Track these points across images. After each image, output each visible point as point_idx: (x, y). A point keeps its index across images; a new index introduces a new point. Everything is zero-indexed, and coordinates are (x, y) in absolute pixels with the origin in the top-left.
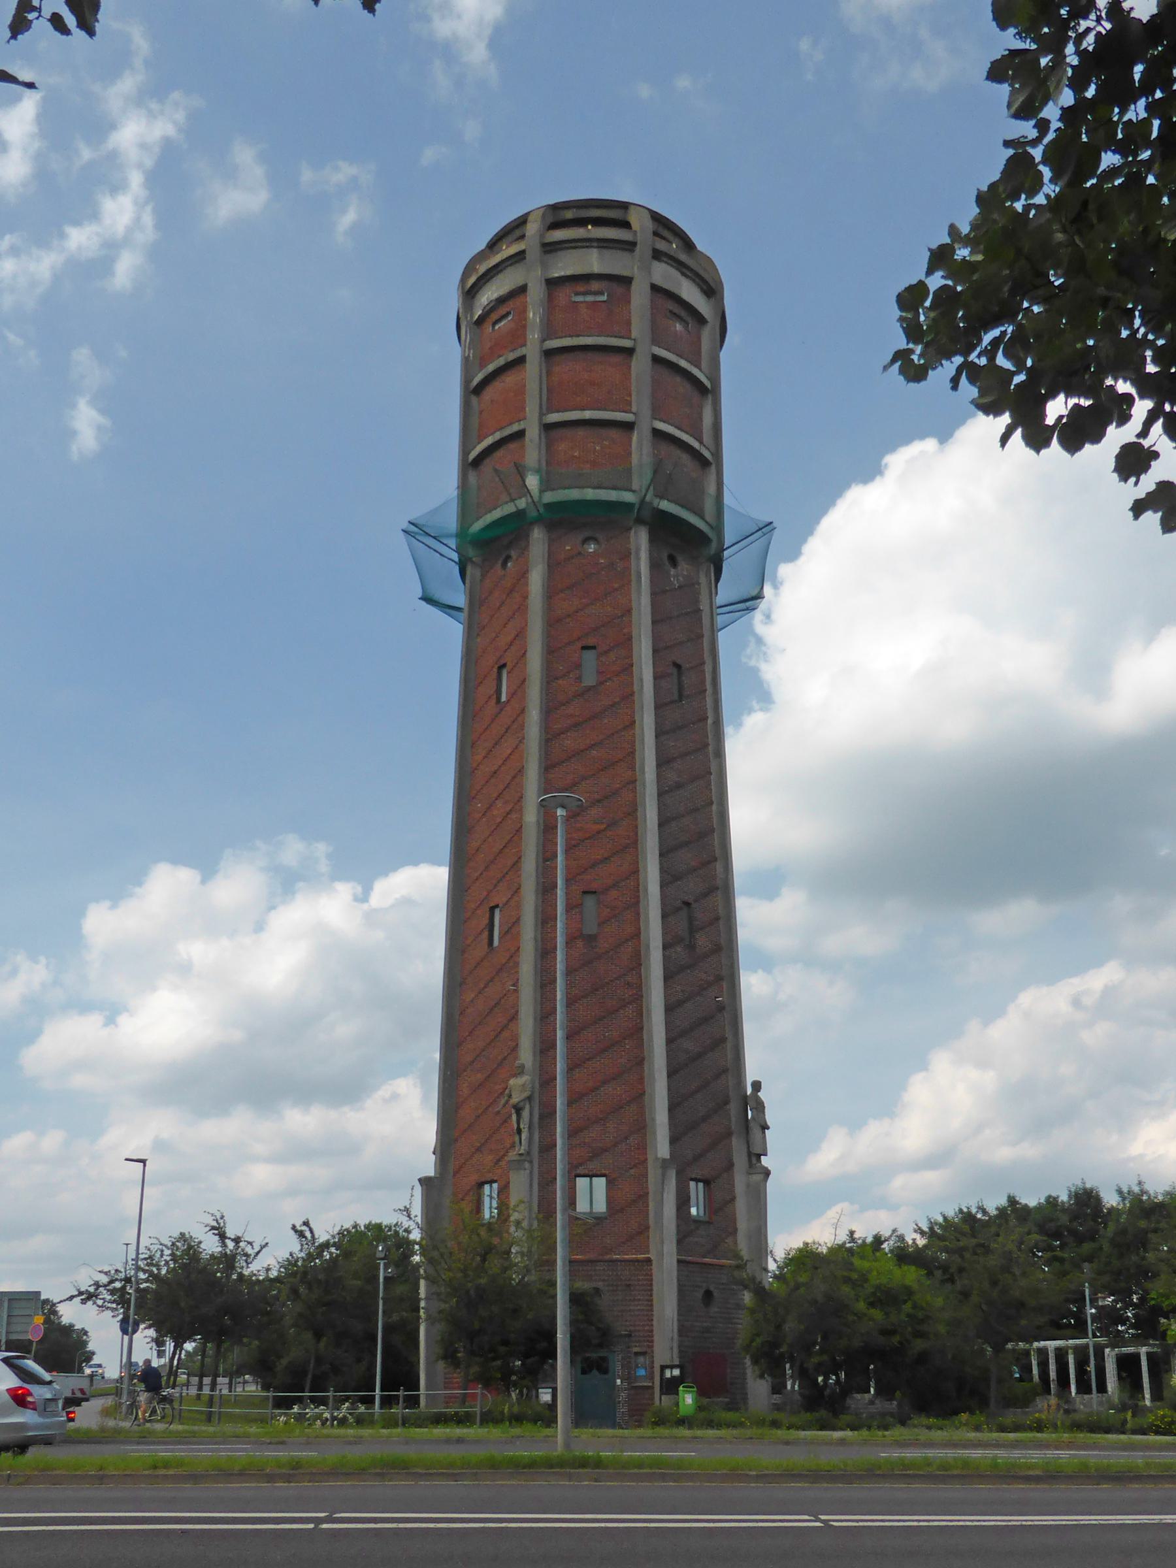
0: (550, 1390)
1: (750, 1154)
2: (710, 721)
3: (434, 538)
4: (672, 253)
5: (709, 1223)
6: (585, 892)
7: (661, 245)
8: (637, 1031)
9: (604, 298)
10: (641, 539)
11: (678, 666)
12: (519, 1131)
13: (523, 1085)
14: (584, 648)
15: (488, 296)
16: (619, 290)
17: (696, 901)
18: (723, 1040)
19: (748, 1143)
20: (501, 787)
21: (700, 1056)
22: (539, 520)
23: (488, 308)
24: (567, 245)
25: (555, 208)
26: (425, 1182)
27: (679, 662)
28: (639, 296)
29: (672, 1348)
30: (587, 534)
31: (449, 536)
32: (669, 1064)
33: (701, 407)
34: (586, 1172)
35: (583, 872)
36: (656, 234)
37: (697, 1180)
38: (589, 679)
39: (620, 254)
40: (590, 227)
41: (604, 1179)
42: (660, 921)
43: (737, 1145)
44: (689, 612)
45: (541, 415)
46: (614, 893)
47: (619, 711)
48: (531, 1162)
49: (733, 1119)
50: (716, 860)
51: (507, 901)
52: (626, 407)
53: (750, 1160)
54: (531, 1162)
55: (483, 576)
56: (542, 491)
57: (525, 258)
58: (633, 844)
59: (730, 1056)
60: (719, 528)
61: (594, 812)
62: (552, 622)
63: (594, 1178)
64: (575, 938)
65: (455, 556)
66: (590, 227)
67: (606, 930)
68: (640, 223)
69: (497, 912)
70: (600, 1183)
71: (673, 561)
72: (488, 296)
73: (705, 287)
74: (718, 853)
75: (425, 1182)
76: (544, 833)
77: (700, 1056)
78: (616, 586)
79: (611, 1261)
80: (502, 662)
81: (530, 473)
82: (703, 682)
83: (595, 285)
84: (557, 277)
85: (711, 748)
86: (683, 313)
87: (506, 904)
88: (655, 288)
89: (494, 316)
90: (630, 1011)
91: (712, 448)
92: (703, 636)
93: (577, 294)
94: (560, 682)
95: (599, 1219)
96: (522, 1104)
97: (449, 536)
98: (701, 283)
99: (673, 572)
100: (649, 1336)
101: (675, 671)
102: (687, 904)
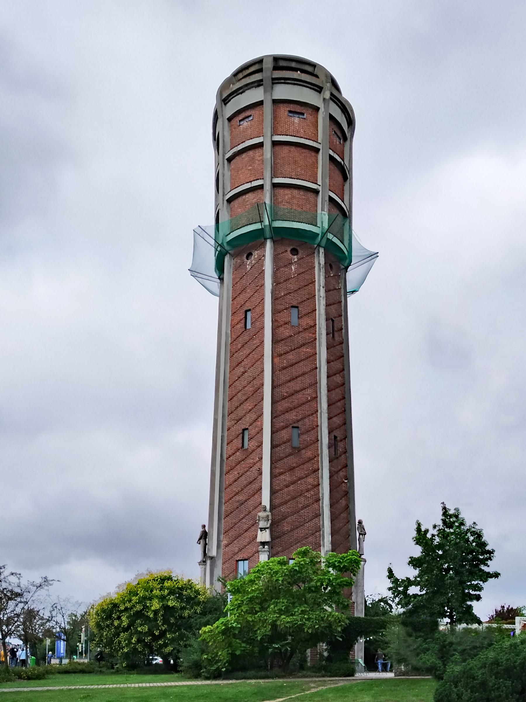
28: (322, 116)
60: (350, 251)
65: (213, 242)
69: (249, 314)
74: (321, 498)
89: (241, 117)
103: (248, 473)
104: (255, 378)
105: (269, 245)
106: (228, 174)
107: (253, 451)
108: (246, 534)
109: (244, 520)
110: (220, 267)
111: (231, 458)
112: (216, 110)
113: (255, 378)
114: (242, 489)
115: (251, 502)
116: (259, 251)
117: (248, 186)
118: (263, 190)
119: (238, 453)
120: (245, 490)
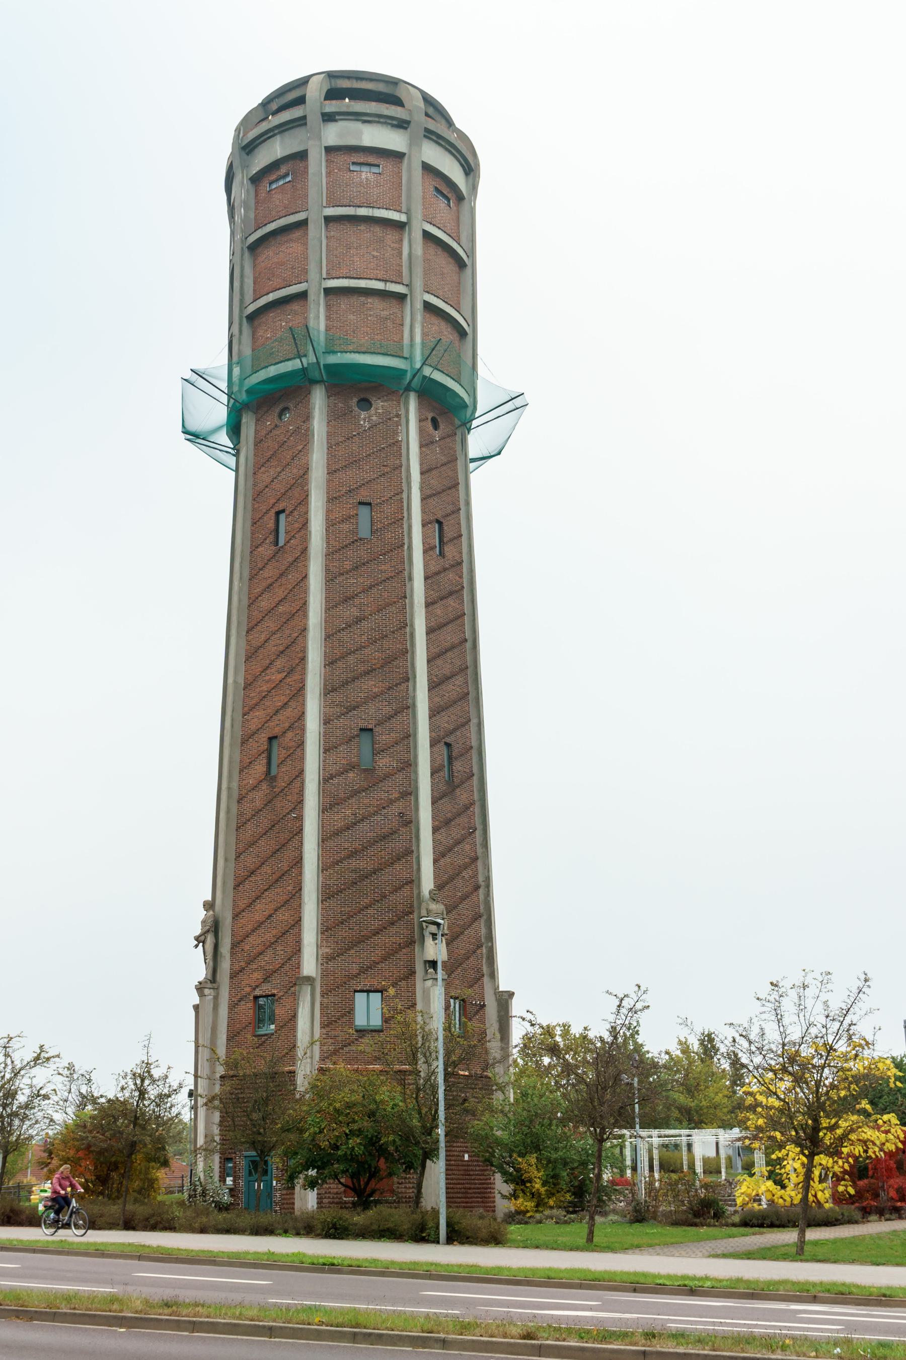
2: (406, 547)
10: (318, 400)
17: (379, 723)
24: (258, 142)
35: (269, 720)
37: (456, 998)
39: (297, 131)
40: (347, 100)
48: (216, 989)
66: (347, 100)
67: (283, 770)
69: (282, 517)
73: (395, 122)
78: (300, 448)
83: (283, 170)
84: (256, 173)
88: (329, 150)
98: (390, 122)
99: (363, 415)
100: (450, 1165)
103: (378, 818)
104: (386, 636)
105: (318, 400)
106: (248, 271)
107: (387, 776)
108: (376, 939)
109: (370, 911)
110: (234, 430)
111: (336, 781)
112: (232, 162)
113: (386, 636)
114: (365, 848)
115: (387, 877)
116: (386, 404)
117: (379, 285)
118: (307, 300)
119: (351, 775)
120: (371, 851)
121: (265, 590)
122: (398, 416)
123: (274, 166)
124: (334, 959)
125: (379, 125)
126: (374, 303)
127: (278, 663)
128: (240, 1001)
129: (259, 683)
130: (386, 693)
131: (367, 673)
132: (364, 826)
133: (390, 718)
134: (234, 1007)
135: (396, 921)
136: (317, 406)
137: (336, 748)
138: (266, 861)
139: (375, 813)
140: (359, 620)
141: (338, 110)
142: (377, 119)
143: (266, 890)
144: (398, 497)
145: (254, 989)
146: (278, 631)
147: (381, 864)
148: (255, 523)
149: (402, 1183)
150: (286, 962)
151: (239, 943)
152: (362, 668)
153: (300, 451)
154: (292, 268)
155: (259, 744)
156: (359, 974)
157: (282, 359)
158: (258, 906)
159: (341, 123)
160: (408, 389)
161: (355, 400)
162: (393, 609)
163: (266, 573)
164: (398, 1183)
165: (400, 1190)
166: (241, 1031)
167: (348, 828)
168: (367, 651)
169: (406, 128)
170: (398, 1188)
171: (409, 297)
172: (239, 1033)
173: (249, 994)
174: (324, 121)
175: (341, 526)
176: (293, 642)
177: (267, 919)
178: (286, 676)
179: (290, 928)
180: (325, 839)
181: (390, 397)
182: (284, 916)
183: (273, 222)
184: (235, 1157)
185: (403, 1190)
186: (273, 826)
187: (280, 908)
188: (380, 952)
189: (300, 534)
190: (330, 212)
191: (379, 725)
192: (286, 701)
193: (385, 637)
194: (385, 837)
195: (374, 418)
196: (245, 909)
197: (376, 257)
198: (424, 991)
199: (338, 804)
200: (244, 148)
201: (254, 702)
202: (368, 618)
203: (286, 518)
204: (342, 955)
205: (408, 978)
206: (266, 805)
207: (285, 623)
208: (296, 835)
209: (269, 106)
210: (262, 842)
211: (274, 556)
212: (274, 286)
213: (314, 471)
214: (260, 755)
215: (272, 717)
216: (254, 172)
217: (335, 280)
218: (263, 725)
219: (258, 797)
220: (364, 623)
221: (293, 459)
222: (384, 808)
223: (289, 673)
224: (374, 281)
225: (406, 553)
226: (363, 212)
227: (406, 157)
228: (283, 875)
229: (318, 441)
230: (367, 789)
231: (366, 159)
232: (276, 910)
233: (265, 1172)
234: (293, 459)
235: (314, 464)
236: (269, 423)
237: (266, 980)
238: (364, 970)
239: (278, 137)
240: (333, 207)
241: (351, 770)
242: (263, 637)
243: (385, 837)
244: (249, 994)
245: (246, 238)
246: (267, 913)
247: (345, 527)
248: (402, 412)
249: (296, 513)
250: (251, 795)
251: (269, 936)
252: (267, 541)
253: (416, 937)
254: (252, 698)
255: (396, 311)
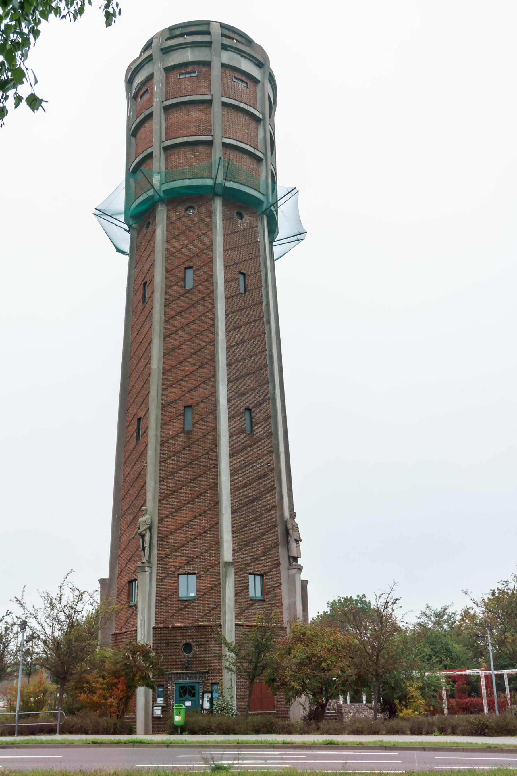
0: (160, 708)
1: (289, 557)
2: (264, 304)
3: (109, 216)
4: (234, 46)
5: (263, 600)
6: (185, 407)
7: (226, 41)
8: (215, 486)
9: (196, 74)
10: (218, 205)
11: (244, 274)
12: (144, 549)
13: (145, 521)
14: (186, 268)
15: (138, 81)
16: (204, 69)
18: (273, 488)
19: (288, 550)
20: (144, 350)
21: (256, 498)
22: (161, 200)
23: (137, 88)
24: (173, 48)
25: (171, 29)
26: (102, 581)
27: (243, 271)
29: (231, 680)
30: (187, 205)
31: (119, 214)
32: (232, 505)
33: (257, 129)
34: (184, 572)
36: (223, 35)
37: (255, 574)
38: (189, 285)
39: (203, 49)
40: (186, 36)
41: (195, 576)
42: (228, 421)
43: (282, 551)
44: (251, 243)
45: (161, 142)
46: (202, 406)
47: (205, 302)
48: (150, 567)
49: (279, 536)
50: (268, 383)
51: (145, 414)
52: (209, 132)
53: (289, 561)
54: (150, 567)
55: (138, 234)
56: (162, 184)
57: (152, 59)
58: (213, 376)
59: (277, 498)
61: (191, 360)
62: (169, 256)
63: (189, 576)
64: (179, 433)
66: (186, 36)
67: (197, 427)
68: (216, 30)
70: (193, 578)
71: (241, 217)
72: (138, 81)
75: (102, 581)
76: (163, 374)
77: (256, 498)
78: (204, 232)
79: (198, 626)
80: (144, 281)
81: (155, 174)
82: (260, 281)
83: (190, 69)
85: (265, 319)
86: (243, 78)
87: (144, 416)
88: (223, 65)
89: (141, 93)
90: (210, 474)
91: (263, 152)
92: (260, 256)
93: (180, 74)
94: (173, 288)
95: (191, 601)
96: (144, 532)
97: (119, 214)
99: (239, 221)
101: (241, 277)
102: (249, 410)
103: (256, 465)
107: (260, 439)
109: (255, 523)
114: (251, 483)
115: (262, 502)
116: (250, 218)
121: (178, 314)
122: (257, 227)
123: (186, 65)
124: (238, 552)
125: (249, 61)
126: (245, 158)
127: (190, 360)
128: (166, 577)
129: (175, 371)
130: (257, 388)
131: (248, 374)
132: (250, 469)
133: (260, 404)
134: (162, 580)
135: (269, 531)
136: (218, 210)
137: (234, 417)
138: (186, 485)
139: (255, 462)
140: (243, 342)
141: (230, 44)
142: (249, 57)
143: (186, 504)
144: (258, 274)
145: (178, 569)
146: (189, 340)
147: (259, 494)
148: (169, 272)
149: (279, 701)
150: (205, 552)
151: (164, 538)
152: (245, 371)
153: (204, 234)
154: (198, 126)
155: (177, 409)
156: (251, 563)
157: (191, 177)
158: (180, 514)
159: (229, 52)
160: (263, 213)
161: (235, 212)
162: (258, 339)
163: (179, 303)
164: (277, 701)
165: (278, 706)
166: (168, 597)
167: (242, 469)
168: (247, 361)
169: (260, 68)
170: (277, 704)
171: (264, 161)
172: (166, 598)
173: (174, 572)
174: (222, 48)
175: (231, 283)
176: (202, 349)
177: (188, 523)
178: (197, 369)
179: (207, 530)
180: (233, 473)
181: (252, 215)
182: (202, 522)
183: (186, 96)
184: (167, 684)
185: (280, 706)
186: (191, 463)
187: (198, 516)
188: (261, 550)
189: (207, 283)
190: (225, 100)
191: (255, 407)
192: (197, 384)
193: (255, 355)
194: (260, 477)
195: (245, 225)
196: (169, 515)
197: (247, 133)
198: (288, 576)
199: (236, 453)
200: (162, 50)
201: (171, 382)
202: (247, 342)
203: (194, 272)
204: (242, 550)
205: (276, 567)
206: (184, 449)
207: (195, 336)
208: (210, 470)
209: (174, 31)
210: (181, 473)
211: (185, 294)
212: (184, 133)
213: (218, 246)
214: (178, 416)
215: (186, 393)
216: (169, 65)
217: (229, 139)
218: (180, 398)
219: (178, 443)
220: (245, 344)
221: (198, 238)
222: (260, 459)
223: (199, 367)
224: (249, 146)
225: (264, 307)
226: (242, 105)
227: (260, 83)
228: (200, 495)
229: (219, 230)
230: (251, 446)
231: (241, 77)
232: (195, 517)
233: (194, 695)
234: (198, 238)
235: (218, 244)
236: (177, 213)
237: (188, 563)
238: (254, 561)
239: (189, 49)
240: (227, 97)
241: (242, 433)
242: (177, 343)
243: (260, 477)
244: (174, 572)
245: (163, 102)
246: (187, 519)
247: (233, 284)
248: (259, 225)
249: (201, 270)
250: (171, 442)
251: (190, 534)
252: (179, 284)
253: (280, 542)
254: (170, 380)
255: (256, 167)
